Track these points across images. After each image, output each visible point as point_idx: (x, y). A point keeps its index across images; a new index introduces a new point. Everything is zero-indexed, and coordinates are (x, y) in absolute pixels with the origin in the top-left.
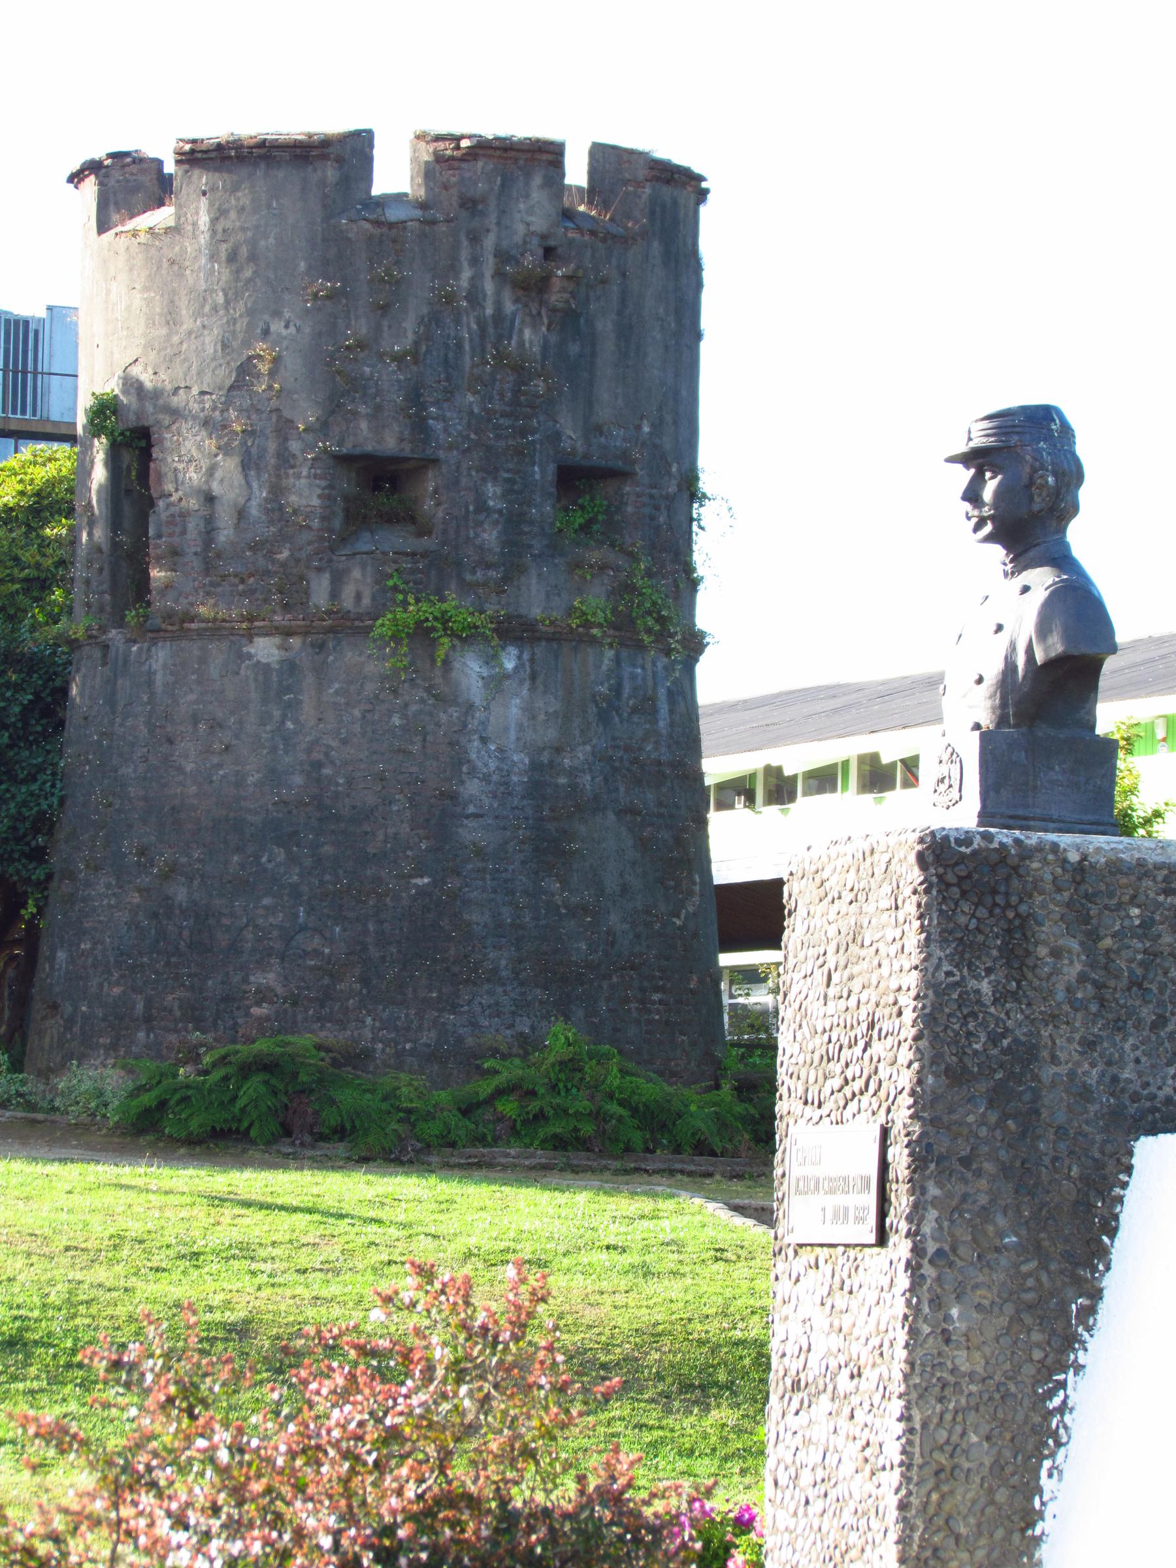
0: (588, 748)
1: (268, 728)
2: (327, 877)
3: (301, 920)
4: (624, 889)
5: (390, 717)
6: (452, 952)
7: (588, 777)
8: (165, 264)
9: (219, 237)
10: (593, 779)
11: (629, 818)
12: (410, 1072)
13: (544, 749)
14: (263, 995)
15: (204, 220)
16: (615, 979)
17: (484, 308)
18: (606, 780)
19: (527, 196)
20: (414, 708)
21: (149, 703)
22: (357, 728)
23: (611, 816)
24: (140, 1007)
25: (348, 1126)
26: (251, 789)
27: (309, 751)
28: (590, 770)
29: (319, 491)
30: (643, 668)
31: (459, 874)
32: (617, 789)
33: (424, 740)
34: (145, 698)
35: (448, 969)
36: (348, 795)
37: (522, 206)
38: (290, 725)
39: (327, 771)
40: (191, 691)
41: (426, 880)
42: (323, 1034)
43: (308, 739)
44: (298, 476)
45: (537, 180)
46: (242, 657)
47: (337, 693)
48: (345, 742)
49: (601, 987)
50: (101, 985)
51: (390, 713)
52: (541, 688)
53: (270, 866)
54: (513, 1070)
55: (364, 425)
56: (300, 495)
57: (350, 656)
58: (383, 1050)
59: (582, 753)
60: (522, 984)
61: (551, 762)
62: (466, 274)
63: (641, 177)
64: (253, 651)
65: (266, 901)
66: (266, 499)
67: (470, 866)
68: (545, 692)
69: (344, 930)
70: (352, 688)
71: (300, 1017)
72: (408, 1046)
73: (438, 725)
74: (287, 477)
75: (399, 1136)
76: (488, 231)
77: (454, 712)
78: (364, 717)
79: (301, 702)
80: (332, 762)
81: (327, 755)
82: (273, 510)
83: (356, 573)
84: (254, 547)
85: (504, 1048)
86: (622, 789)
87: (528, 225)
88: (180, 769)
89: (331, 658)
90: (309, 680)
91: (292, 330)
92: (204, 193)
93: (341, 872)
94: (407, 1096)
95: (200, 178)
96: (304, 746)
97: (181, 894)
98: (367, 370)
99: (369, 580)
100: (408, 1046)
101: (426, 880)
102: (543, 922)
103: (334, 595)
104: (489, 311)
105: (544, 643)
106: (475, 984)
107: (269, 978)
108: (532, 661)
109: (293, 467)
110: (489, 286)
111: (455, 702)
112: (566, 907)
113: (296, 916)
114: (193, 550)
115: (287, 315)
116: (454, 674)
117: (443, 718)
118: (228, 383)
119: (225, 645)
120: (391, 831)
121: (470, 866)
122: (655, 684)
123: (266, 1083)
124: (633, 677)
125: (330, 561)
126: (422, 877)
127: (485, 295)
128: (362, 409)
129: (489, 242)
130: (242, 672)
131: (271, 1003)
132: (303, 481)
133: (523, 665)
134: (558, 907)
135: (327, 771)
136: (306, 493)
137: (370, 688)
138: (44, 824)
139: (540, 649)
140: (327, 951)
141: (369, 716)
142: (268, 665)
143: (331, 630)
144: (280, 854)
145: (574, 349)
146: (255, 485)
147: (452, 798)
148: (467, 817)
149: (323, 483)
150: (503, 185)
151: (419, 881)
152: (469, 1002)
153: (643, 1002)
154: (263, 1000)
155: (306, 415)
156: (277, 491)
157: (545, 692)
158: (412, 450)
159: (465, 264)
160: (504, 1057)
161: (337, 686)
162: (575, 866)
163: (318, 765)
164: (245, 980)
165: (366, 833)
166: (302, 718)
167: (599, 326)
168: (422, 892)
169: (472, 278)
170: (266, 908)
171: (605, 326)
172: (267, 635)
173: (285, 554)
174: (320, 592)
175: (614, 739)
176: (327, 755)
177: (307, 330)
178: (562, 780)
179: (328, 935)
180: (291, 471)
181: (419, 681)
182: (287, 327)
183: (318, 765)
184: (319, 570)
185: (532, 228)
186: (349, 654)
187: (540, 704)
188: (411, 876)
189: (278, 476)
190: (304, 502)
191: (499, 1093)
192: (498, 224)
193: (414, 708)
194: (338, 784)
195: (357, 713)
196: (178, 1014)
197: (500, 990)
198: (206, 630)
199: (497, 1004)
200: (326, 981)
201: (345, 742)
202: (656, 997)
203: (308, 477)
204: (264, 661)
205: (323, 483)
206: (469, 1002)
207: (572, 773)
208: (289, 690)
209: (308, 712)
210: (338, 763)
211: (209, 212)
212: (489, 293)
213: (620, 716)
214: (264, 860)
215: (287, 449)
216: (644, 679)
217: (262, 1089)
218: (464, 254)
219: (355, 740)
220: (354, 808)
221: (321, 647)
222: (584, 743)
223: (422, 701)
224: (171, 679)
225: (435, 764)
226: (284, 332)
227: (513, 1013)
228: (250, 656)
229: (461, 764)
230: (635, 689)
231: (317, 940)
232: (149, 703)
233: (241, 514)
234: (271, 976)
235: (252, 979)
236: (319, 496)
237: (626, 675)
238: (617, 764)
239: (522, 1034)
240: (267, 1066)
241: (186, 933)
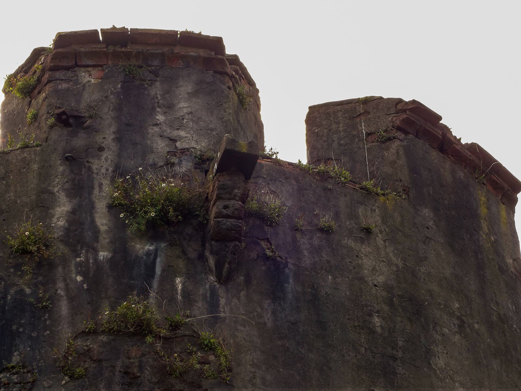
17: (96, 251)
37: (160, 118)
87: (173, 141)
127: (96, 232)
159: (62, 197)
192: (118, 139)
212: (103, 228)
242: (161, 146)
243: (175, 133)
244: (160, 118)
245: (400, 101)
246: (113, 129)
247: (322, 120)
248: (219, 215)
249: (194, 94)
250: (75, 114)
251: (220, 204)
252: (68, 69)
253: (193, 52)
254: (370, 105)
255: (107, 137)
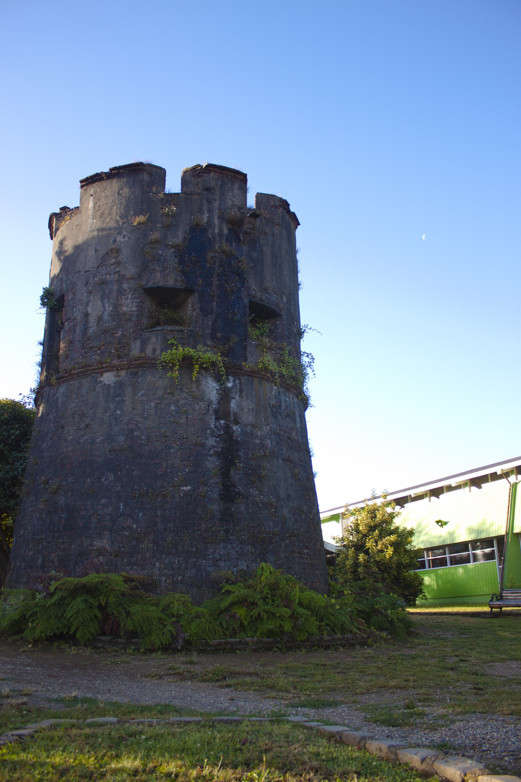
0: (268, 427)
1: (108, 414)
2: (136, 487)
3: (121, 510)
4: (289, 497)
5: (170, 406)
6: (203, 526)
7: (269, 441)
8: (75, 227)
9: (97, 209)
10: (271, 442)
11: (288, 463)
12: (181, 593)
13: (248, 425)
14: (101, 552)
15: (91, 205)
16: (287, 542)
17: (214, 230)
18: (277, 443)
19: (233, 191)
20: (182, 402)
21: (55, 412)
22: (153, 412)
23: (281, 462)
24: (40, 561)
25: (139, 630)
26: (98, 445)
27: (128, 424)
28: (270, 438)
29: (136, 304)
30: (289, 399)
31: (206, 485)
32: (282, 449)
33: (187, 417)
34: (54, 411)
35: (201, 535)
36: (147, 445)
37: (230, 194)
38: (118, 412)
39: (136, 433)
40: (73, 402)
41: (189, 488)
42: (131, 572)
43: (127, 418)
44: (126, 299)
45: (236, 186)
46: (97, 383)
47: (142, 395)
48: (146, 418)
49: (281, 545)
50: (25, 551)
51: (169, 405)
52: (245, 397)
53: (106, 483)
54: (239, 591)
55: (158, 275)
56: (127, 307)
57: (150, 378)
58: (166, 580)
59: (266, 429)
60: (241, 543)
61: (251, 431)
62: (206, 215)
63: (277, 205)
64: (102, 379)
65: (103, 501)
66: (111, 311)
67: (212, 481)
68: (247, 399)
69: (144, 515)
70: (150, 393)
71: (119, 563)
72: (179, 578)
73: (195, 410)
74: (122, 300)
75: (172, 634)
76: (216, 200)
77: (203, 405)
78: (156, 406)
79: (125, 401)
80: (140, 429)
81: (137, 425)
82: (114, 315)
83: (154, 340)
84: (105, 332)
85: (233, 578)
86: (284, 449)
87: (233, 202)
88: (66, 440)
89: (140, 379)
90: (129, 390)
91: (126, 238)
92: (92, 195)
93: (143, 484)
94: (177, 607)
95: (91, 190)
96: (125, 421)
97: (62, 501)
98: (160, 252)
99: (159, 342)
100: (179, 578)
101: (189, 488)
102: (251, 511)
103: (142, 350)
104: (216, 231)
105: (245, 377)
106: (216, 543)
107: (103, 543)
108: (240, 384)
109: (124, 295)
110: (216, 222)
111: (202, 400)
112: (262, 504)
113: (119, 508)
114: (78, 339)
115: (124, 233)
116: (202, 387)
117: (197, 407)
118: (96, 265)
119: (90, 379)
120: (170, 462)
121: (212, 481)
122: (294, 407)
123: (85, 601)
124: (286, 401)
125: (141, 335)
126: (186, 486)
127: (215, 225)
128: (158, 268)
129: (216, 204)
130: (97, 390)
131: (104, 556)
132: (129, 300)
133: (236, 385)
134: (258, 503)
135: (136, 433)
136: (129, 305)
137: (160, 392)
138: (16, 482)
139: (244, 379)
140: (135, 526)
141: (159, 406)
142: (109, 385)
143: (141, 366)
144: (111, 477)
145: (255, 255)
146: (107, 305)
147: (201, 446)
148: (210, 456)
149: (138, 301)
150: (222, 184)
151: (185, 488)
152: (213, 553)
153: (300, 553)
154: (100, 554)
155: (131, 270)
156: (116, 306)
157: (247, 399)
158: (181, 285)
159: (206, 212)
160: (233, 583)
161: (143, 392)
162: (265, 483)
163: (132, 431)
164: (91, 545)
165: (157, 464)
166: (125, 408)
167: (265, 249)
168: (186, 493)
169: (209, 217)
170: (103, 505)
171: (267, 250)
172: (109, 371)
173: (120, 333)
174: (135, 350)
175: (279, 426)
176: (137, 425)
177: (133, 238)
178: (257, 441)
179: (135, 518)
180: (123, 297)
181: (184, 390)
182: (124, 238)
183: (132, 431)
184: (135, 339)
185: (235, 203)
186: (149, 377)
187: (244, 404)
188: (180, 486)
189: (118, 300)
190: (129, 310)
191: (233, 604)
192: (220, 198)
193: (182, 402)
194: (142, 440)
195: (152, 404)
196: (57, 564)
197: (230, 546)
198: (81, 373)
199: (228, 554)
200: (134, 543)
201: (146, 418)
202: (306, 551)
203: (132, 298)
204: (107, 383)
205: (138, 301)
206: (213, 553)
207: (262, 439)
208: (119, 395)
209: (128, 405)
210: (142, 429)
211: (93, 201)
212: (216, 224)
213: (281, 416)
214: (103, 480)
215: (122, 288)
216: (290, 403)
217: (82, 606)
218: (205, 208)
219: (151, 417)
220: (150, 451)
221: (135, 374)
222: (266, 425)
223: (186, 398)
224: (65, 399)
225: (193, 429)
226: (123, 240)
227: (237, 558)
228: (101, 382)
229: (206, 429)
230: (287, 406)
231: (129, 520)
232: (55, 412)
233: (100, 319)
234: (105, 541)
235: (95, 543)
236: (136, 307)
237: (283, 400)
238: (282, 437)
239: (242, 570)
240: (90, 590)
241: (63, 520)
242: (230, 202)
243: (234, 199)
244: (230, 194)
245: (282, 199)
246: (219, 195)
247: (260, 197)
248: (247, 228)
249: (239, 189)
250: (483, 536)
251: (248, 225)
252: (207, 173)
253: (239, 176)
254: (273, 197)
255: (217, 196)
